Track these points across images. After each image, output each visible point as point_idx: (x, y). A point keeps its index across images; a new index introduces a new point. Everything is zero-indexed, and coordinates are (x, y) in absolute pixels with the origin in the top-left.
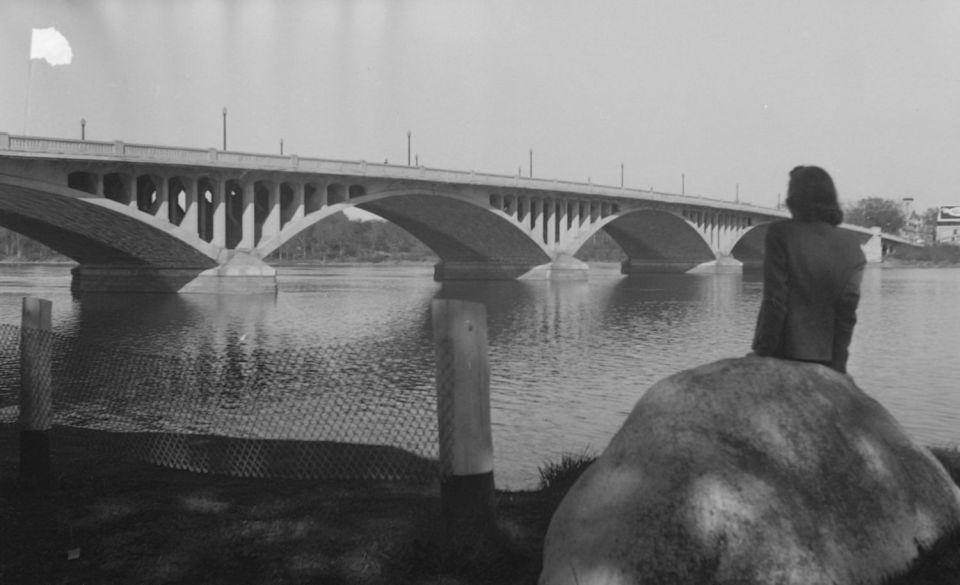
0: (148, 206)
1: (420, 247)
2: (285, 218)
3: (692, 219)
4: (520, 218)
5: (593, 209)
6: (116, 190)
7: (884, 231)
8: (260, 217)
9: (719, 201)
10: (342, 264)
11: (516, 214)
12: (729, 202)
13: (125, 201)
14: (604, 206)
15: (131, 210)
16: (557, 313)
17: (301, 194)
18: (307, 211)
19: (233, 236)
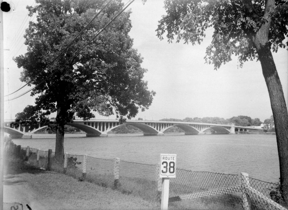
0: (93, 126)
1: (182, 130)
2: (165, 128)
3: (227, 129)
4: (154, 128)
5: (204, 127)
6: (152, 125)
7: (106, 62)
8: (107, 127)
9: (105, 120)
10: (189, 133)
11: (95, 126)
12: (107, 120)
13: (90, 126)
14: (167, 125)
15: (91, 127)
16: (117, 17)
17: (113, 124)
18: (167, 127)
19: (200, 130)
